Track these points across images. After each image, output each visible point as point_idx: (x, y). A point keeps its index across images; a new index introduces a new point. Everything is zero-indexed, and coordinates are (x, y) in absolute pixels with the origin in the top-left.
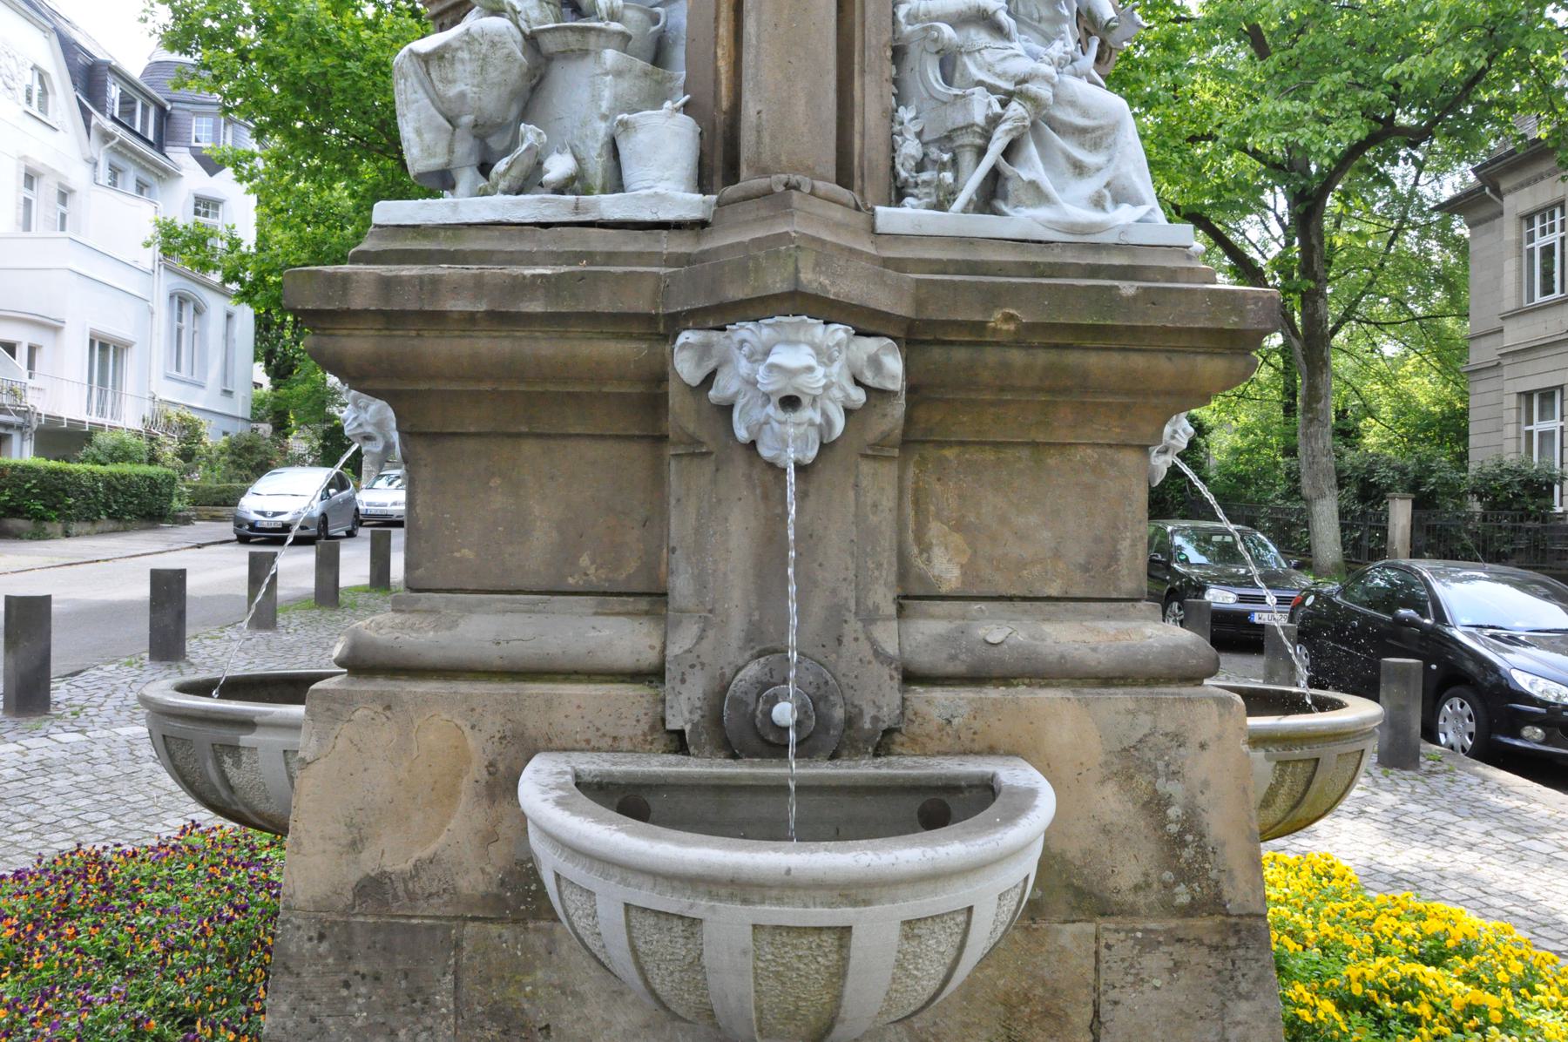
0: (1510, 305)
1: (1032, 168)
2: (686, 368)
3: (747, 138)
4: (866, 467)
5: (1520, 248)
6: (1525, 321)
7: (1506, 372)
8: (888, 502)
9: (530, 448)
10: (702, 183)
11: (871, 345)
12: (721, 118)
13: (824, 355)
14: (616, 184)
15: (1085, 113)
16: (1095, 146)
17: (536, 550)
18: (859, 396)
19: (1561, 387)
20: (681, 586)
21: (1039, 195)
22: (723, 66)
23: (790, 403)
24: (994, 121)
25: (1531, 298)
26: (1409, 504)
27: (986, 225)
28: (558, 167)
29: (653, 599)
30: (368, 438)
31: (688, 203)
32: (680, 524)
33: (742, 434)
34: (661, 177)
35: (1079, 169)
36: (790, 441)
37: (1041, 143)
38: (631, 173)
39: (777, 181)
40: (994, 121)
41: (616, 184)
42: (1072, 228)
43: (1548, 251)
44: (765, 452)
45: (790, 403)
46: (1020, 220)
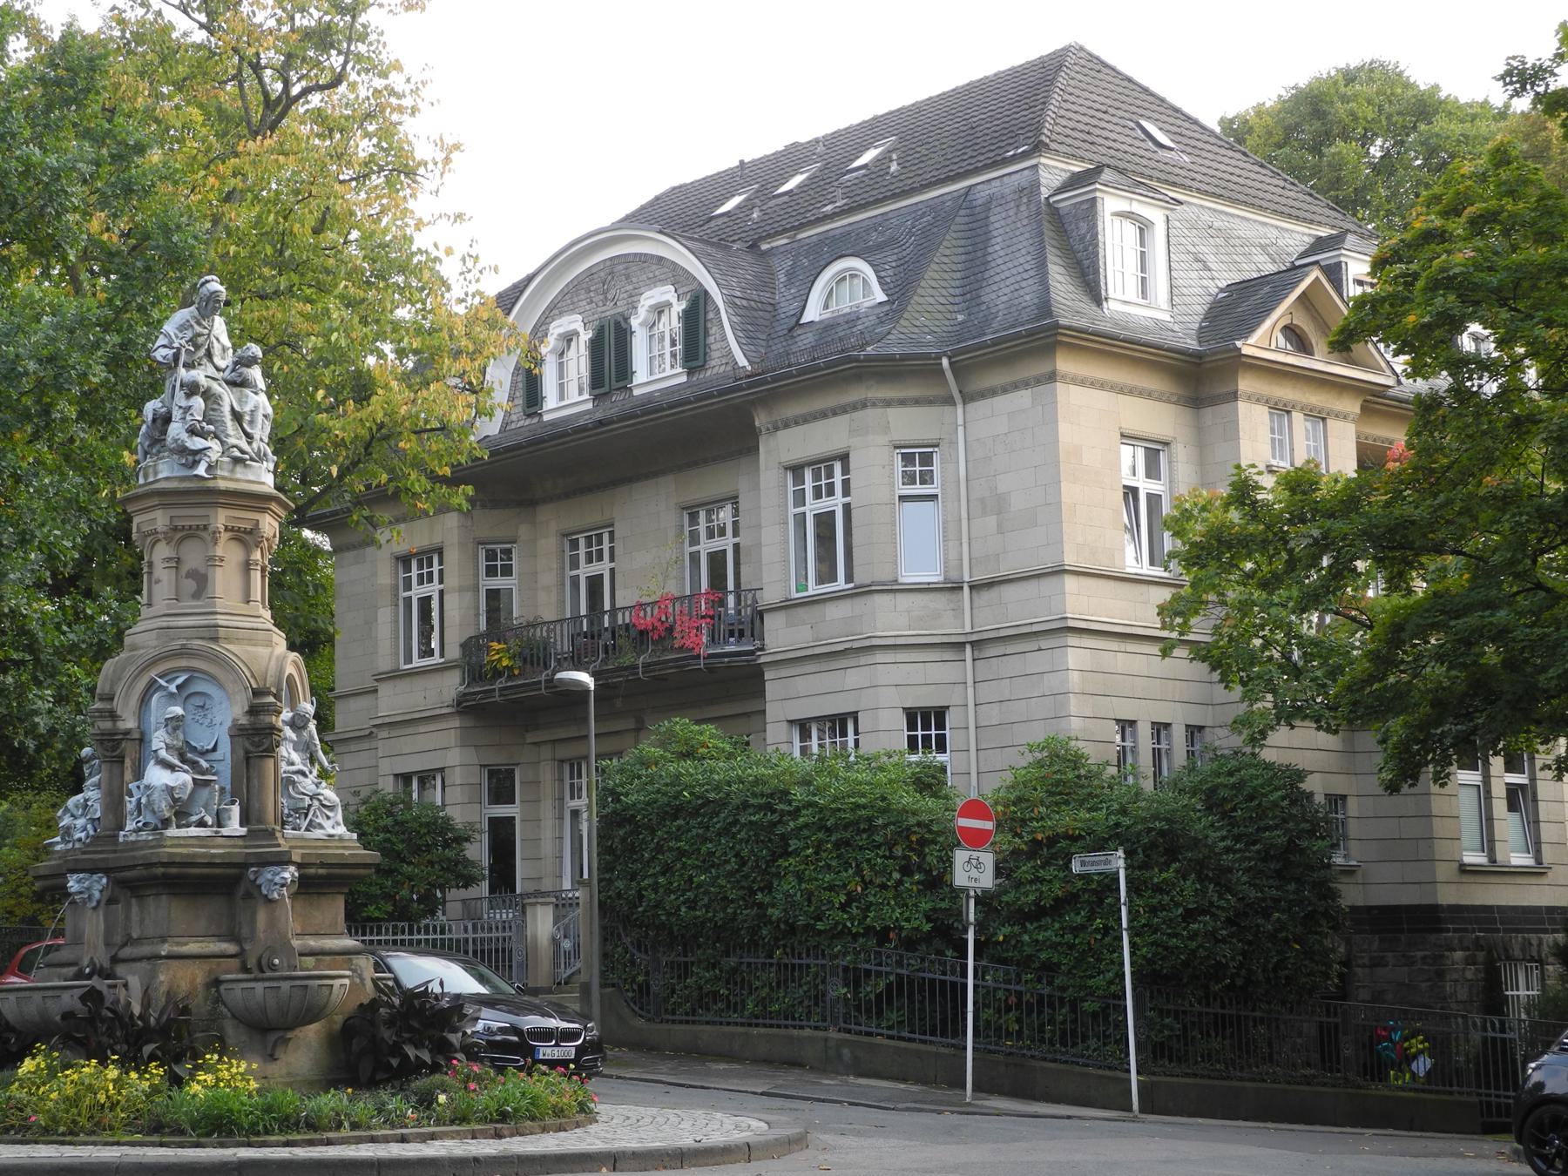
0: (384, 664)
5: (396, 595)
6: (402, 685)
7: (383, 747)
11: (95, 877)
19: (442, 770)
21: (321, 826)
25: (409, 660)
26: (550, 910)
27: (309, 835)
34: (234, 827)
43: (425, 602)
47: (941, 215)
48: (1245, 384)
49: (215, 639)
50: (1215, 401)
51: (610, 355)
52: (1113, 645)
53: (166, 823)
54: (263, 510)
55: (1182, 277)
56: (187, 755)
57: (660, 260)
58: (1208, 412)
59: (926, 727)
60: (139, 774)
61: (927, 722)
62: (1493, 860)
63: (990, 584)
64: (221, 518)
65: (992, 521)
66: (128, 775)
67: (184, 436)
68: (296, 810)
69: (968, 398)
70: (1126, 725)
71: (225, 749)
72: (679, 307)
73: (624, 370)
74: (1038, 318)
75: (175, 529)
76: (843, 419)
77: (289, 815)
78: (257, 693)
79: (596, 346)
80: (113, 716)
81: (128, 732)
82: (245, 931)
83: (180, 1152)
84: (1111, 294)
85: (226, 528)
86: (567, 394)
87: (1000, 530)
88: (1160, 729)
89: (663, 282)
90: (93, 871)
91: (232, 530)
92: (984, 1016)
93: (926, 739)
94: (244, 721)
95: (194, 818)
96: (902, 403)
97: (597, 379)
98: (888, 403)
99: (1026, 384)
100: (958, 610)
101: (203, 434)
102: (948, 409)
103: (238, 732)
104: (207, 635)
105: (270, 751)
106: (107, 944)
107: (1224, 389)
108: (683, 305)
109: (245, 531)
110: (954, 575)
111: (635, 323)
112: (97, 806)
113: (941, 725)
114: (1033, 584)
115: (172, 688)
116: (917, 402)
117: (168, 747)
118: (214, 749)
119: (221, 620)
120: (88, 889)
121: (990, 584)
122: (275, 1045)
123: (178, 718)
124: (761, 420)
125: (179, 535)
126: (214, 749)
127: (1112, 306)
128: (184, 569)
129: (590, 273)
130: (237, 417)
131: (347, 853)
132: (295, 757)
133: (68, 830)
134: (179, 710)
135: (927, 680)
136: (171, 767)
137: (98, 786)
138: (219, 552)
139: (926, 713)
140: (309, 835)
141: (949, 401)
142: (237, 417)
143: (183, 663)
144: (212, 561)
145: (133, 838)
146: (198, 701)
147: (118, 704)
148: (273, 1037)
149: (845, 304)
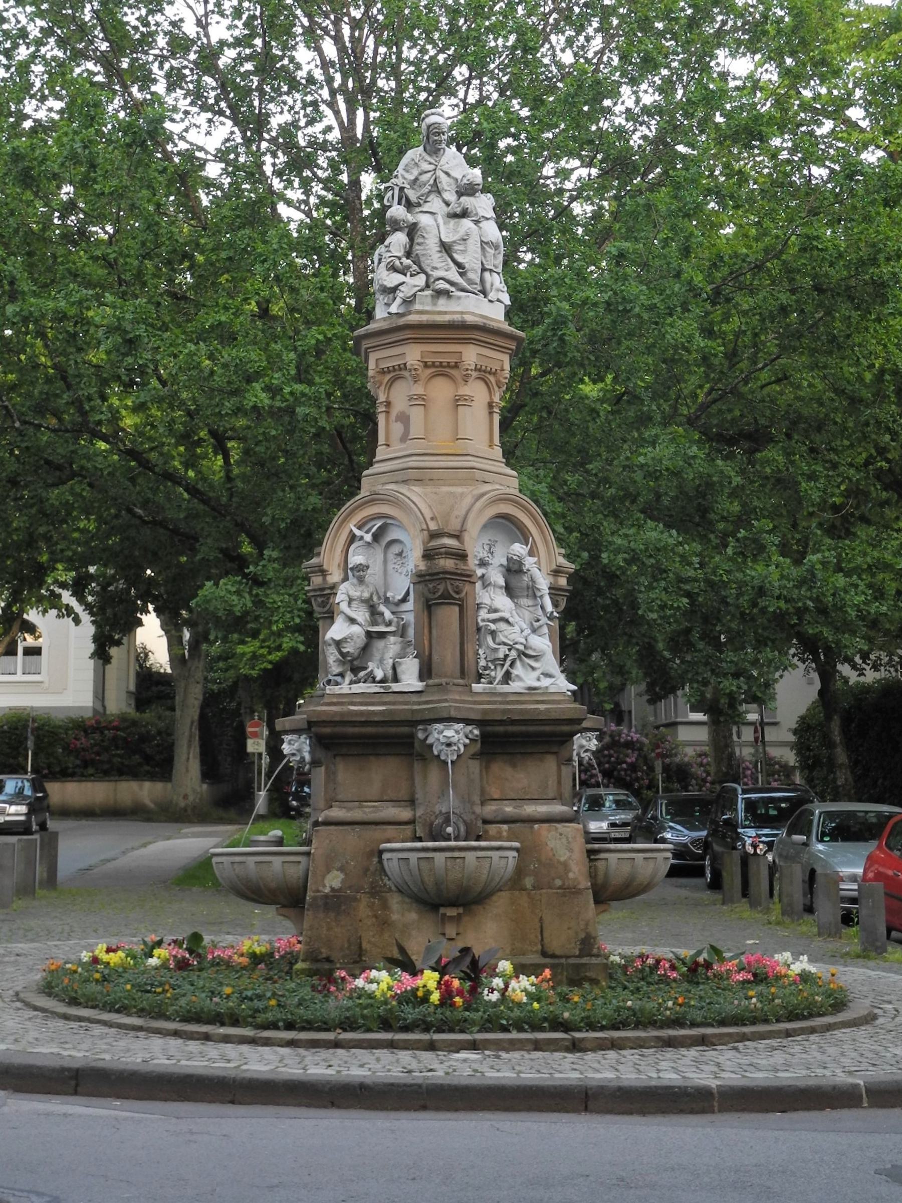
1: (518, 670)
2: (421, 735)
3: (434, 665)
4: (470, 761)
8: (477, 771)
9: (372, 758)
10: (421, 678)
11: (470, 728)
12: (426, 658)
13: (457, 732)
14: (396, 679)
15: (535, 650)
16: (537, 660)
17: (374, 790)
18: (467, 741)
20: (419, 795)
22: (426, 642)
23: (449, 745)
24: (506, 656)
27: (505, 688)
28: (379, 674)
29: (412, 802)
30: (293, 755)
31: (418, 686)
32: (418, 779)
33: (436, 753)
34: (410, 680)
35: (533, 668)
36: (450, 756)
37: (521, 660)
38: (401, 676)
39: (443, 681)
40: (506, 656)
41: (396, 679)
42: (530, 688)
44: (443, 758)
45: (449, 745)
46: (515, 686)
77: (486, 668)
78: (434, 535)
91: (433, 365)
94: (422, 566)
104: (400, 478)
109: (449, 365)
115: (368, 538)
120: (299, 750)
125: (388, 377)
130: (446, 248)
131: (542, 707)
140: (505, 688)
146: (396, 549)
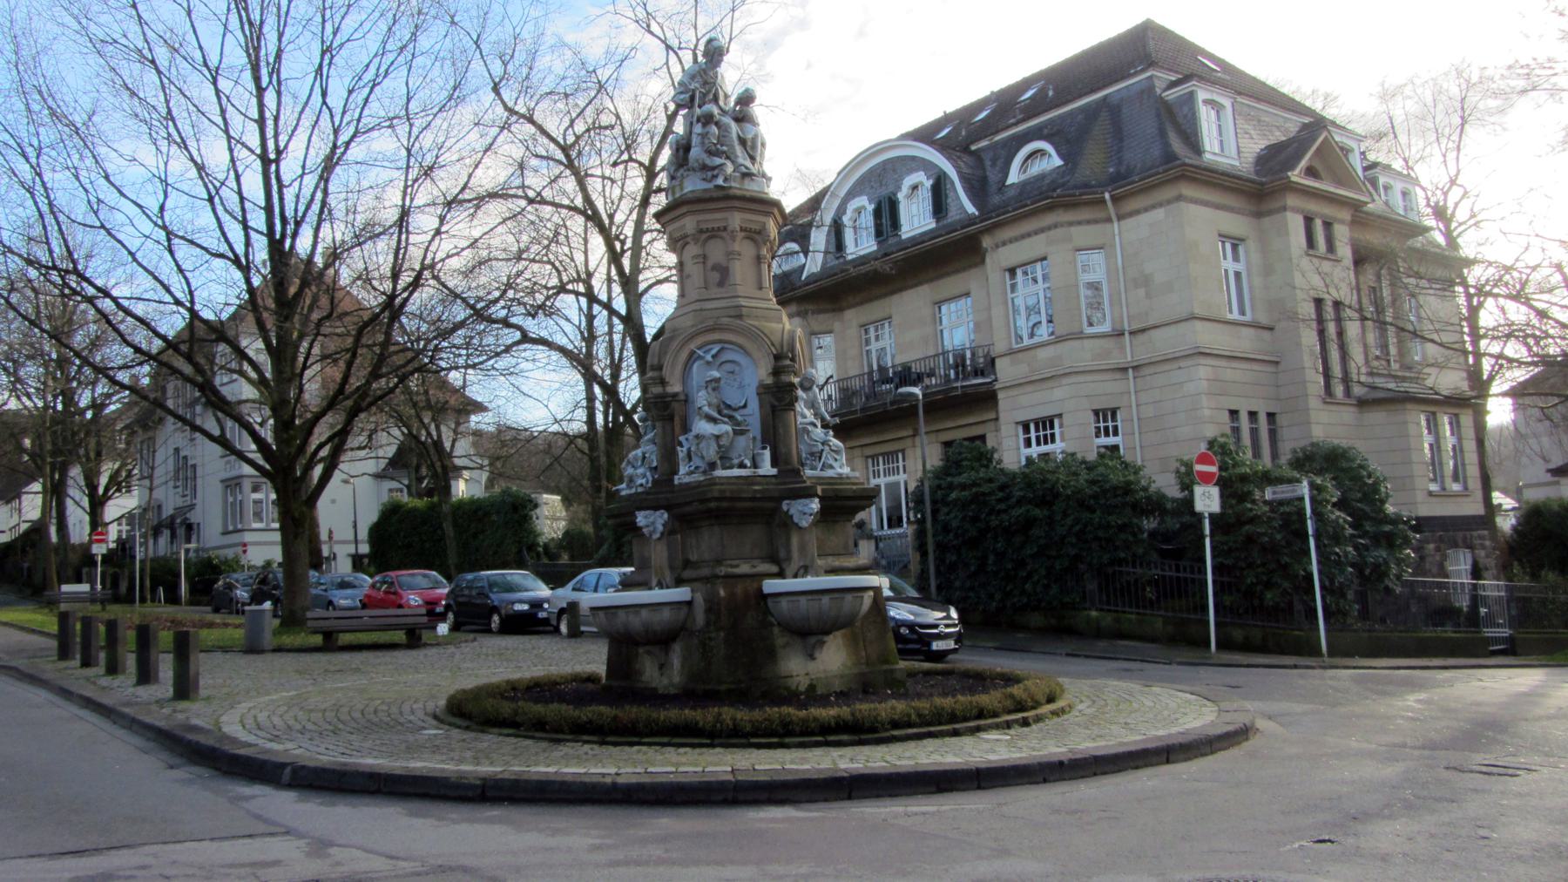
21: (831, 467)
34: (767, 469)
47: (1091, 113)
48: (1291, 200)
49: (740, 317)
50: (1270, 213)
51: (887, 215)
52: (1223, 363)
53: (712, 466)
54: (768, 214)
55: (1244, 142)
56: (725, 411)
57: (913, 158)
58: (1266, 221)
59: (1105, 421)
60: (686, 429)
61: (1106, 416)
62: (1444, 489)
63: (1143, 331)
64: (736, 220)
65: (1141, 292)
66: (677, 429)
67: (705, 156)
68: (812, 454)
69: (1120, 218)
70: (1234, 413)
71: (754, 406)
72: (929, 183)
73: (896, 224)
74: (465, 624)
75: (701, 231)
76: (1042, 236)
79: (877, 213)
80: (663, 382)
81: (675, 395)
82: (782, 554)
83: (924, 809)
84: (1207, 147)
85: (742, 229)
86: (860, 244)
87: (1148, 296)
88: (1253, 415)
89: (917, 170)
90: (656, 508)
92: (1228, 600)
93: (1106, 429)
94: (769, 381)
95: (736, 461)
96: (1079, 223)
97: (879, 233)
98: (1071, 224)
99: (1160, 205)
100: (1122, 348)
101: (718, 154)
102: (1108, 225)
103: (763, 390)
105: (791, 405)
106: (672, 568)
107: (1276, 205)
108: (931, 182)
110: (1118, 327)
111: (900, 196)
112: (654, 457)
113: (1114, 419)
114: (1173, 328)
115: (709, 358)
116: (1089, 222)
117: (710, 405)
118: (745, 406)
119: (743, 302)
121: (1143, 331)
122: (814, 647)
123: (717, 380)
124: (987, 242)
125: (704, 236)
126: (745, 406)
127: (1207, 156)
128: (710, 263)
129: (871, 171)
130: (743, 142)
132: (806, 412)
133: (631, 480)
134: (716, 374)
135: (1107, 390)
136: (714, 420)
137: (653, 441)
138: (737, 247)
139: (1104, 411)
141: (1109, 220)
142: (743, 142)
143: (716, 336)
144: (730, 255)
145: (687, 480)
146: (728, 367)
147: (666, 372)
148: (813, 640)
149: (1038, 167)
